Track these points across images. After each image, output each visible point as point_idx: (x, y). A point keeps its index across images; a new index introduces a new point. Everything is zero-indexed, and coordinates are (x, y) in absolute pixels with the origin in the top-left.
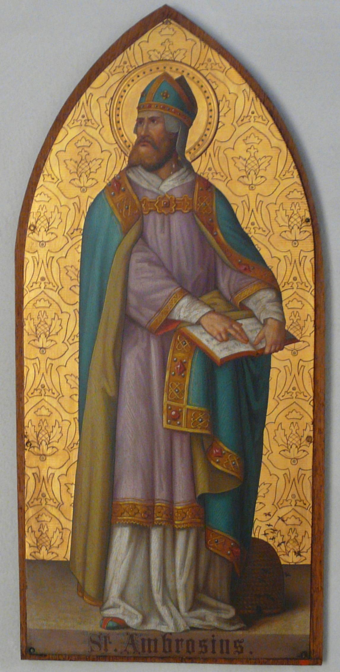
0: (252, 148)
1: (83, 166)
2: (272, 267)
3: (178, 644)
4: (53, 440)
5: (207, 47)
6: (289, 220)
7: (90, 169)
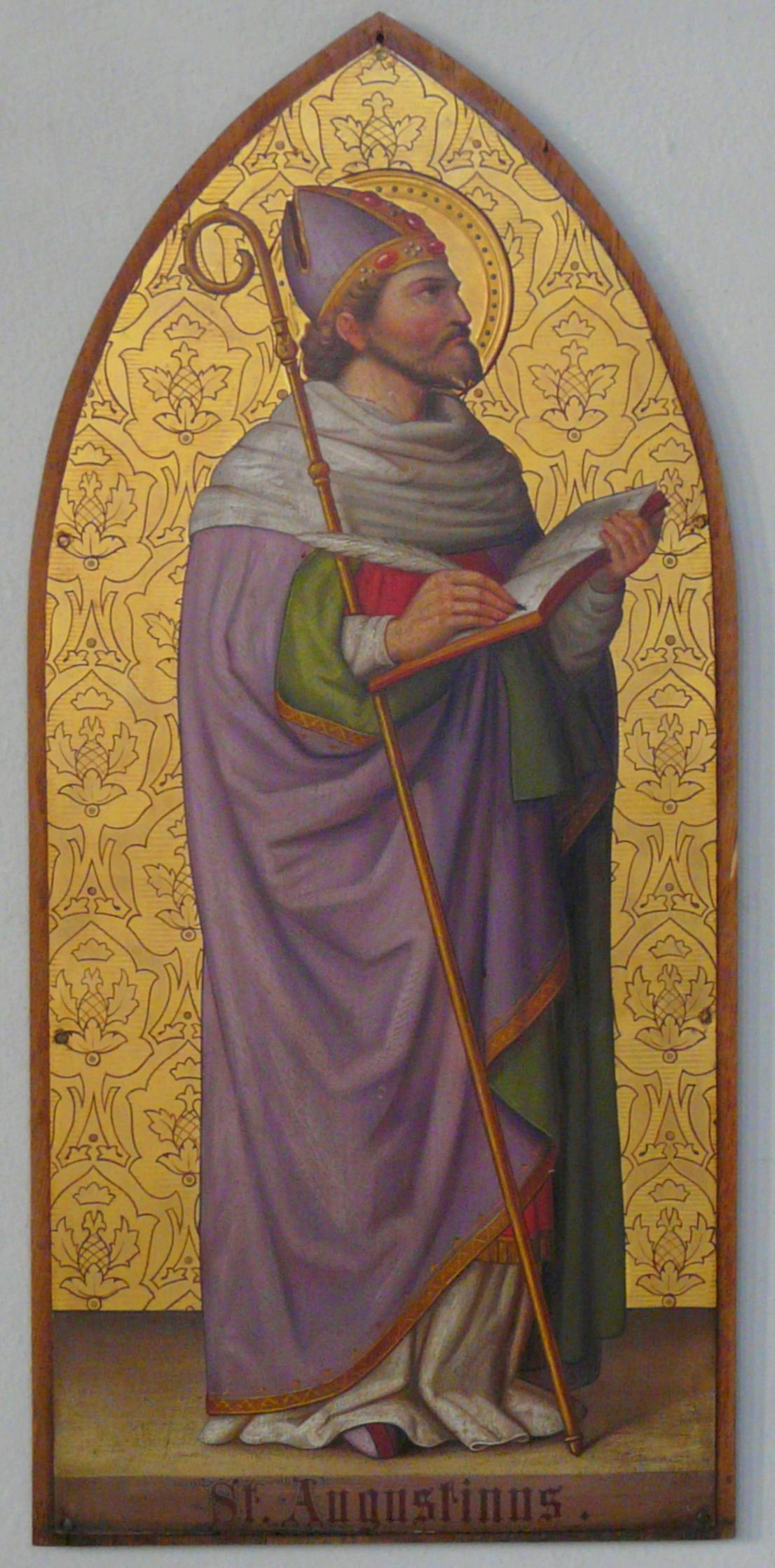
0: (574, 346)
1: (184, 384)
2: (622, 787)
4: (116, 1263)
7: (202, 390)
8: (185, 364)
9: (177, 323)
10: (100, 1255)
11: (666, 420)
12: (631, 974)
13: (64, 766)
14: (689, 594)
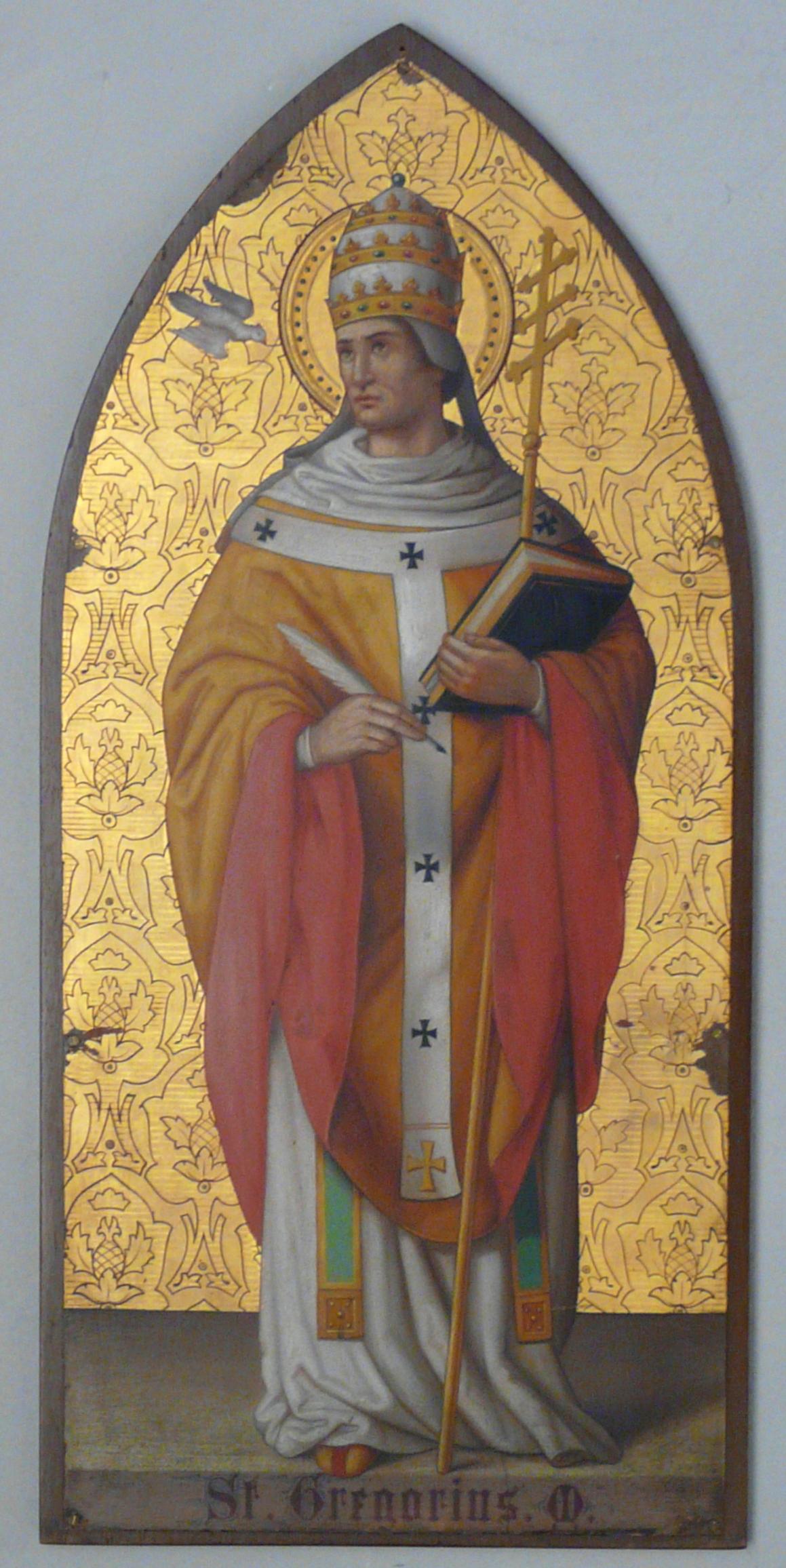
3: (334, 1500)
6: (96, 523)
10: (116, 1261)
11: (685, 438)
12: (650, 497)
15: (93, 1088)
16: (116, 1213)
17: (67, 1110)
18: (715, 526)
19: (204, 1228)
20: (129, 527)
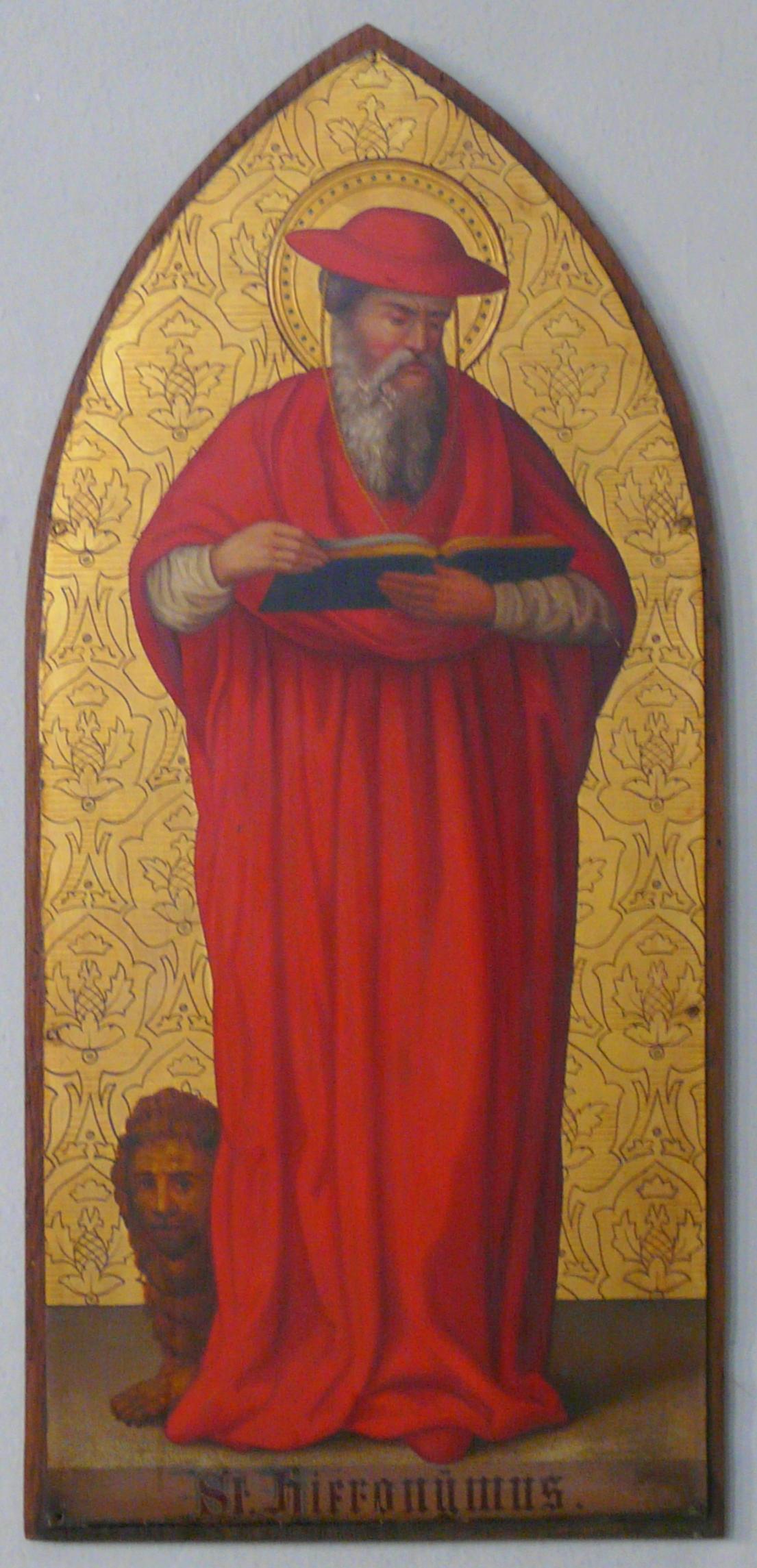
4: (112, 1009)
5: (462, 113)
8: (180, 360)
9: (176, 815)
13: (59, 761)
14: (676, 1087)
15: (71, 583)
16: (98, 1204)
17: (47, 1101)
18: (686, 506)
19: (184, 969)
20: (108, 1003)
